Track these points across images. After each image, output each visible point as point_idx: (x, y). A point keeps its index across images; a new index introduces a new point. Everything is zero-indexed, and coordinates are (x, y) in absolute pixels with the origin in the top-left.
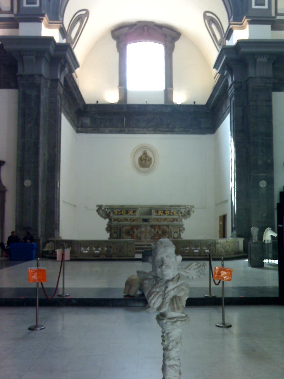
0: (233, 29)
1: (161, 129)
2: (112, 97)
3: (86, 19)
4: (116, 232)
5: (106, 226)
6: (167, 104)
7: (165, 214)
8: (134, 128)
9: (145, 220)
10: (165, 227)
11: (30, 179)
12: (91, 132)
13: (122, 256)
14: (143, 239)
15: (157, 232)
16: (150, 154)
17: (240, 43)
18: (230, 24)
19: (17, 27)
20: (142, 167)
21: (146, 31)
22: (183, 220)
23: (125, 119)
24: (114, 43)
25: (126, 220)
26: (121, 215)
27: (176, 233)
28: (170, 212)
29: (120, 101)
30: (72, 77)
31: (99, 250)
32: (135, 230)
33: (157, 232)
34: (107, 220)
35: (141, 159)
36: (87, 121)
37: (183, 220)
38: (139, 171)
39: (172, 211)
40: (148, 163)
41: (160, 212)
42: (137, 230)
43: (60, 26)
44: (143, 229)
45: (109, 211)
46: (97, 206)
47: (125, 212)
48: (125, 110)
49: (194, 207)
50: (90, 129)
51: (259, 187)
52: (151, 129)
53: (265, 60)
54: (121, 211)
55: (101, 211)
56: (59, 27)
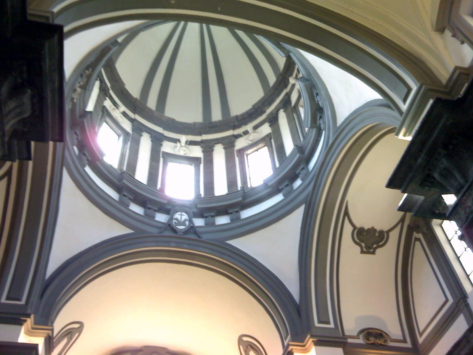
0: (294, 351)
3: (77, 335)
43: (48, 334)
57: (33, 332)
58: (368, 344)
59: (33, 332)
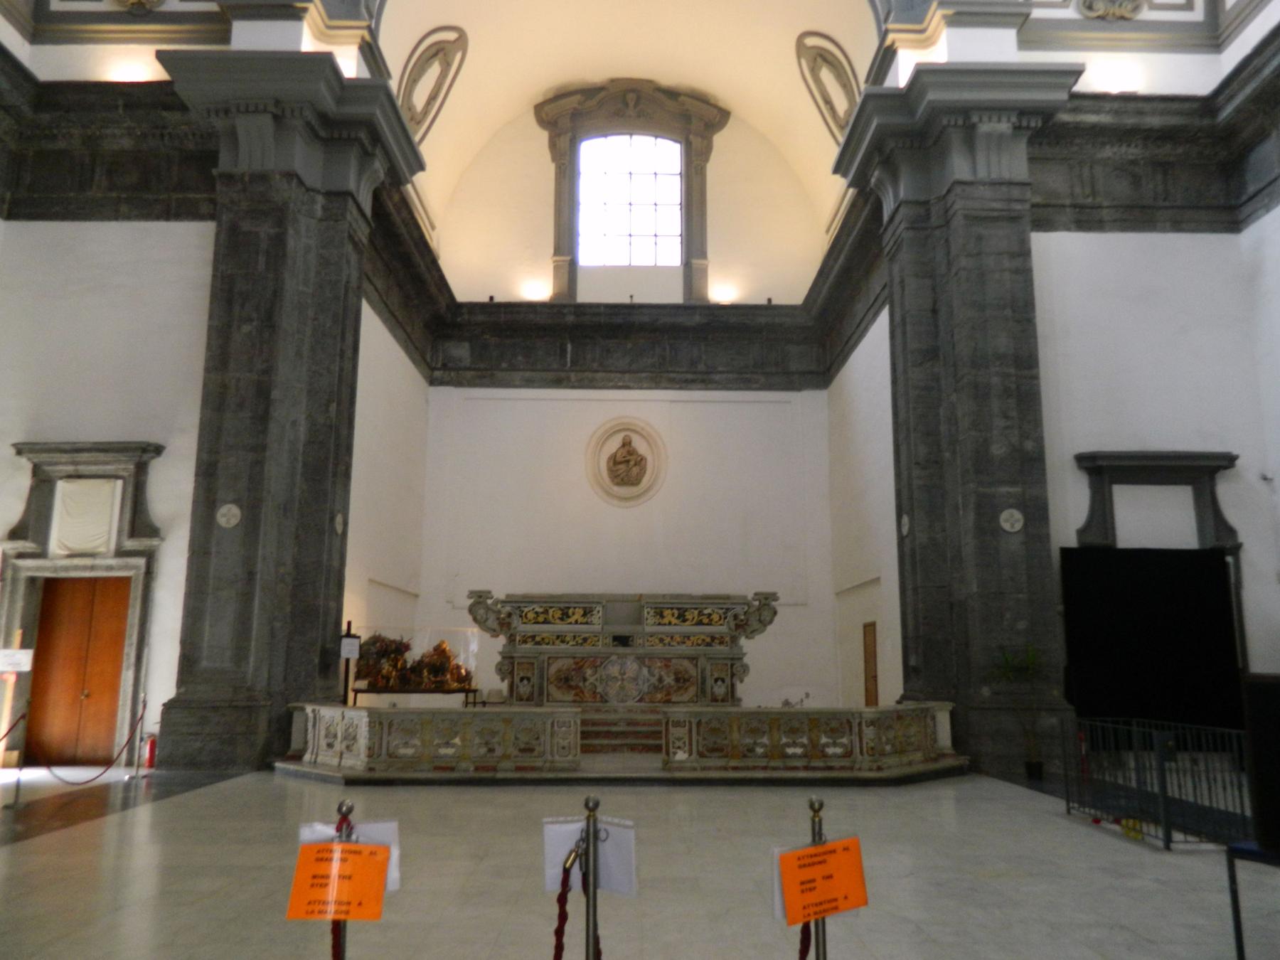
0: (897, 44)
1: (672, 375)
2: (535, 286)
3: (459, 56)
4: (529, 679)
5: (499, 658)
6: (693, 302)
7: (685, 621)
8: (597, 371)
9: (622, 641)
10: (686, 663)
11: (236, 502)
12: (471, 384)
13: (533, 769)
14: (614, 703)
15: (660, 680)
16: (640, 446)
17: (922, 74)
18: (883, 35)
19: (225, 38)
20: (618, 484)
21: (631, 104)
22: (743, 641)
23: (569, 347)
24: (543, 136)
25: (561, 638)
26: (546, 622)
27: (719, 683)
28: (700, 614)
29: (556, 296)
30: (405, 204)
31: (453, 746)
32: (589, 672)
33: (660, 680)
34: (502, 640)
35: (614, 461)
36: (461, 351)
37: (743, 641)
38: (608, 493)
39: (706, 612)
40: (635, 470)
41: (667, 613)
42: (596, 672)
43: (363, 38)
44: (614, 670)
45: (508, 609)
46: (472, 594)
47: (559, 614)
48: (570, 319)
49: (776, 599)
50: (469, 374)
51: (997, 531)
52: (644, 375)
53: (1004, 127)
54: (546, 612)
55: (482, 611)
56: (359, 40)
57: (329, 36)
58: (1087, 18)
59: (329, 36)
